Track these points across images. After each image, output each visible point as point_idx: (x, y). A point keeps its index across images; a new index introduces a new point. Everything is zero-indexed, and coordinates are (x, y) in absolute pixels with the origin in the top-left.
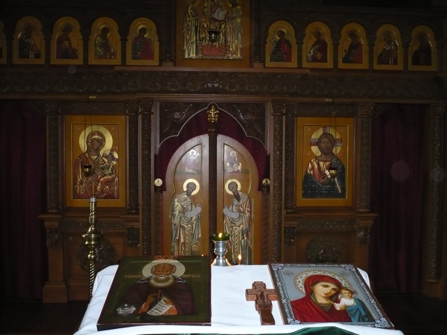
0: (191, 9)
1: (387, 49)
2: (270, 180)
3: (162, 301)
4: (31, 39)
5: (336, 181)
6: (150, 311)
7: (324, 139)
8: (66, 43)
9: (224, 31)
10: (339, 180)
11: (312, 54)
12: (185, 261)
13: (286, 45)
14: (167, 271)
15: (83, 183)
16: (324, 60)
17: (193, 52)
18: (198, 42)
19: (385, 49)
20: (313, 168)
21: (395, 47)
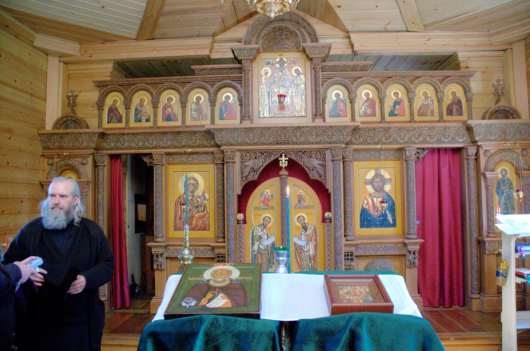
0: (265, 79)
1: (425, 104)
2: (331, 213)
3: (219, 296)
4: (144, 107)
5: (388, 214)
6: (209, 304)
7: (376, 179)
8: (170, 110)
9: (291, 95)
10: (390, 212)
11: (363, 110)
12: (239, 267)
13: (342, 104)
14: (224, 275)
15: (182, 218)
16: (373, 114)
17: (267, 112)
18: (270, 104)
19: (423, 104)
20: (368, 204)
21: (431, 102)
